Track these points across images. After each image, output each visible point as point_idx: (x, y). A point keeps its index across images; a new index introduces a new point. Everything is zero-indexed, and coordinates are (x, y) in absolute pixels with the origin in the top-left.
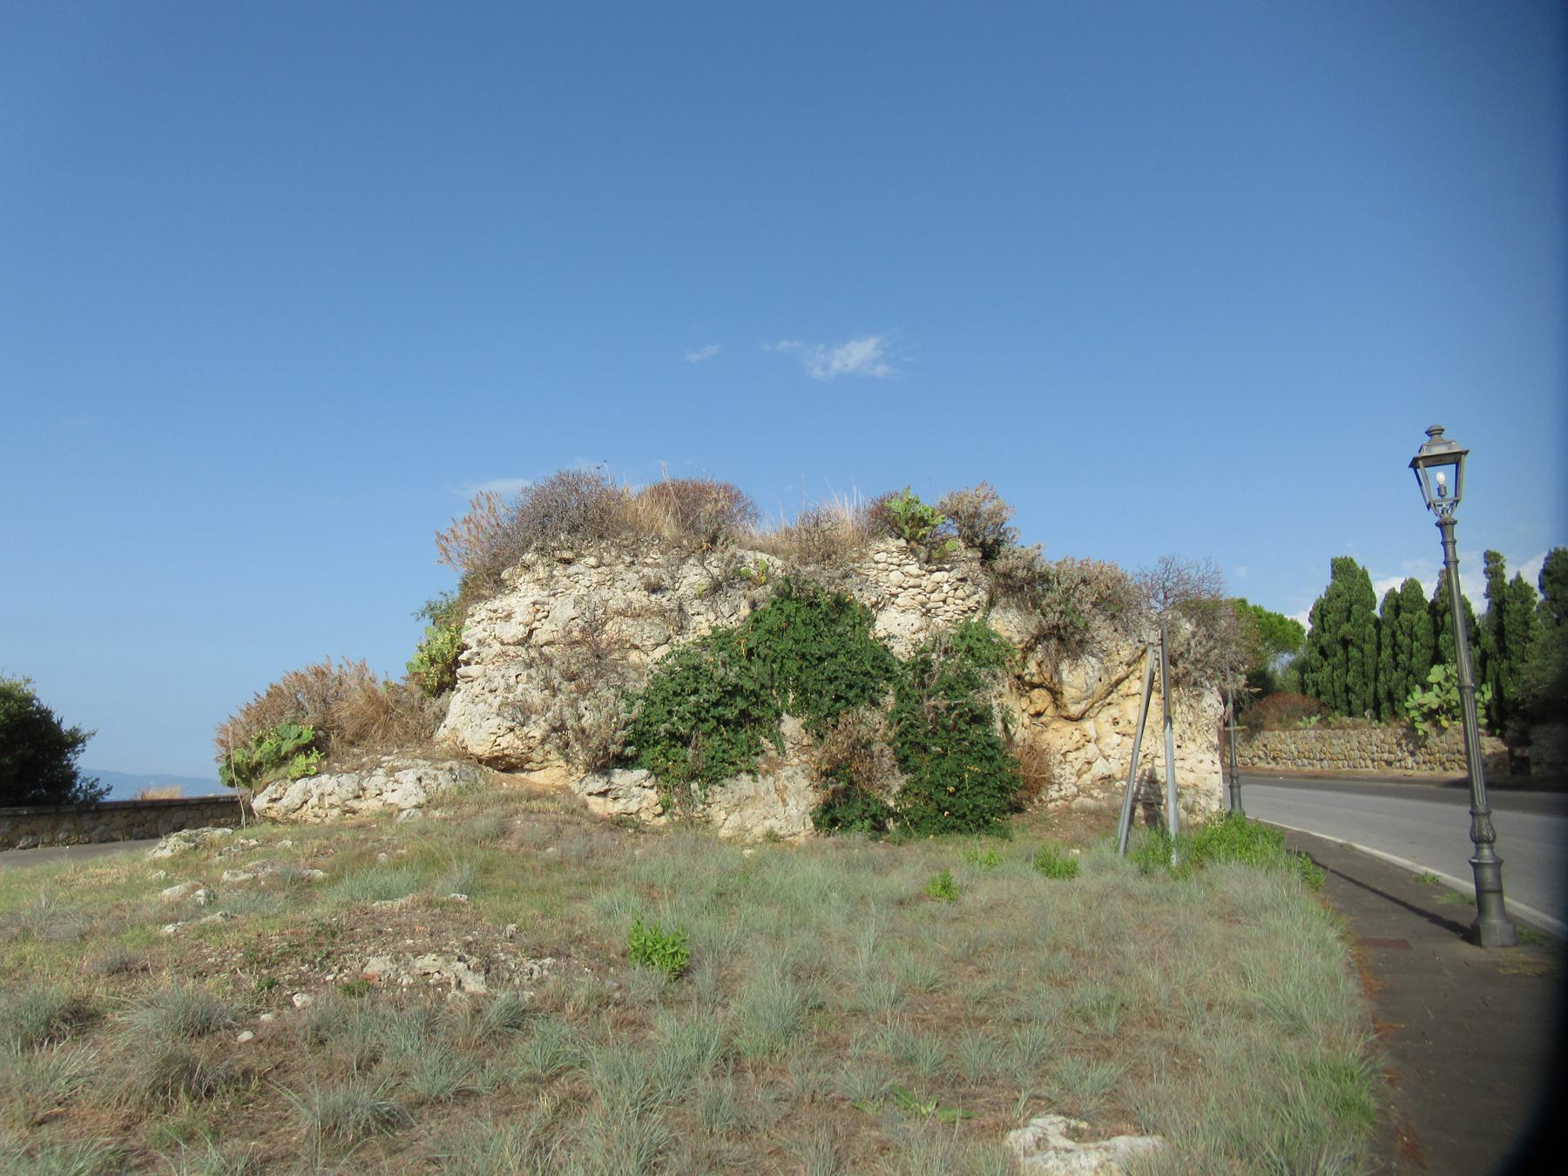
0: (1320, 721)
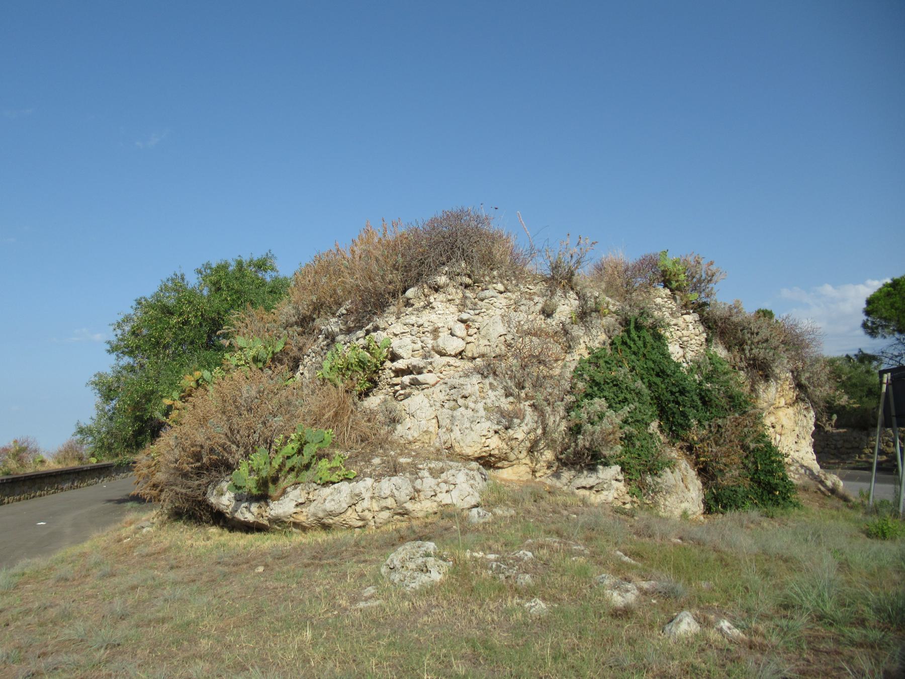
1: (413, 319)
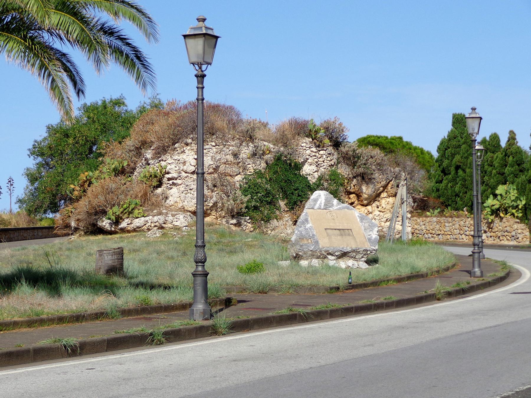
0: (439, 213)
1: (176, 157)
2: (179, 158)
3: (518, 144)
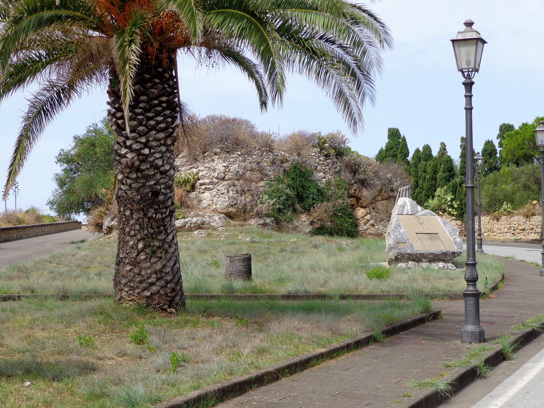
1: (207, 165)
2: (209, 166)
3: (448, 154)
